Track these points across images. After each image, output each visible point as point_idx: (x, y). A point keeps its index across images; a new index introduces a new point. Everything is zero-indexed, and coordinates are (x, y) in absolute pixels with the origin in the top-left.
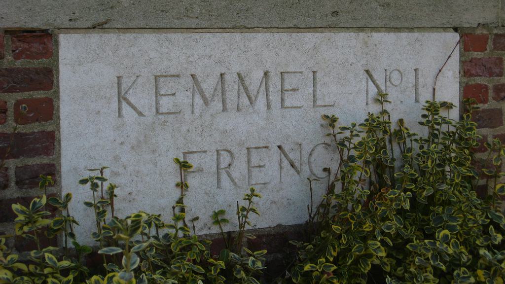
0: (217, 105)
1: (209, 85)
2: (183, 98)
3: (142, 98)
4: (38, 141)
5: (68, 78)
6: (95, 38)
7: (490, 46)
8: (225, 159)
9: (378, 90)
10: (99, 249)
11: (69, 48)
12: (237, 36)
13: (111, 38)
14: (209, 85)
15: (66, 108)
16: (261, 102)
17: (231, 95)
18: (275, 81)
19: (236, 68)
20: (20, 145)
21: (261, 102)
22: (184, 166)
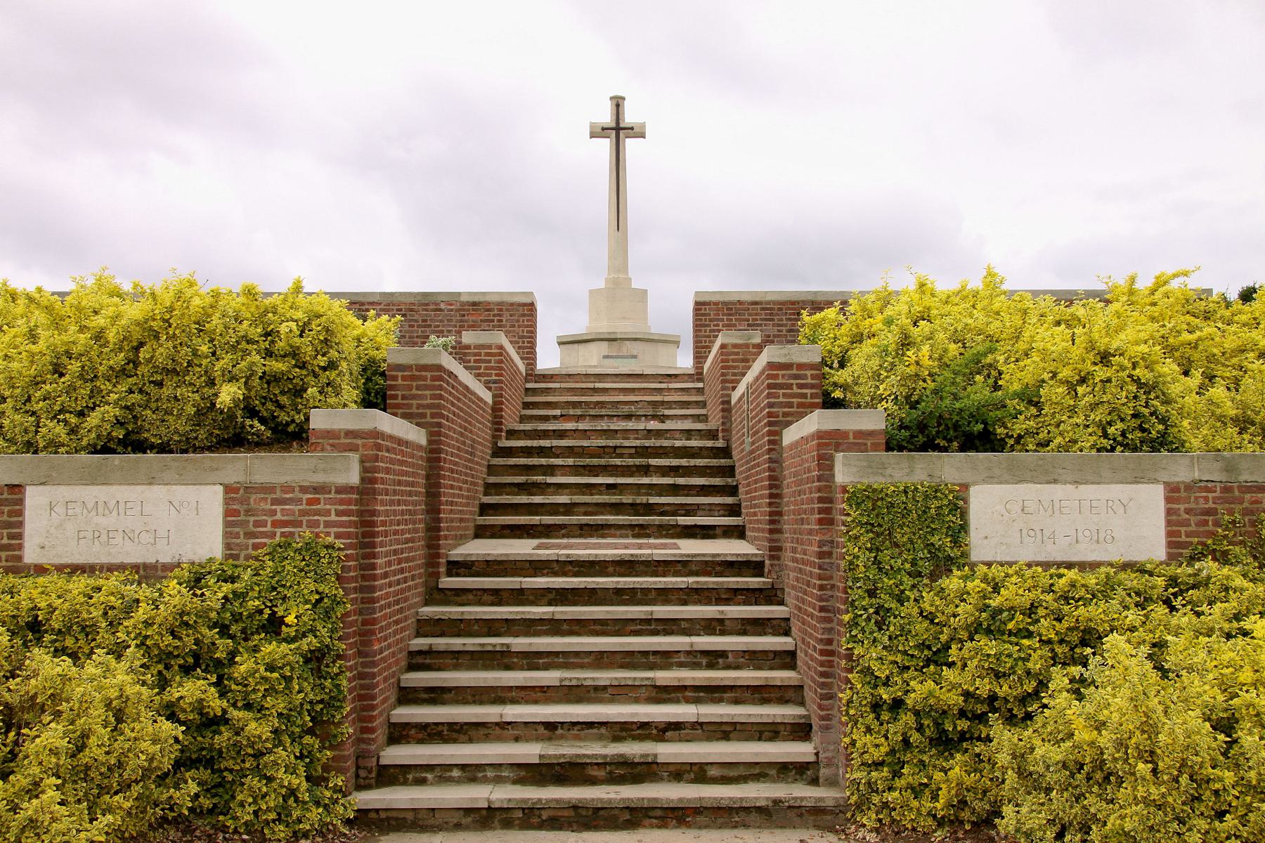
0: (94, 513)
1: (90, 506)
2: (78, 510)
3: (60, 509)
4: (15, 527)
5: (29, 502)
6: (41, 487)
7: (242, 491)
8: (97, 534)
9: (28, 567)
10: (985, 355)
11: (30, 492)
12: (104, 487)
13: (47, 488)
14: (90, 506)
15: (27, 513)
16: (115, 513)
17: (101, 509)
18: (122, 506)
19: (103, 499)
20: (10, 525)
21: (115, 513)
22: (618, 131)
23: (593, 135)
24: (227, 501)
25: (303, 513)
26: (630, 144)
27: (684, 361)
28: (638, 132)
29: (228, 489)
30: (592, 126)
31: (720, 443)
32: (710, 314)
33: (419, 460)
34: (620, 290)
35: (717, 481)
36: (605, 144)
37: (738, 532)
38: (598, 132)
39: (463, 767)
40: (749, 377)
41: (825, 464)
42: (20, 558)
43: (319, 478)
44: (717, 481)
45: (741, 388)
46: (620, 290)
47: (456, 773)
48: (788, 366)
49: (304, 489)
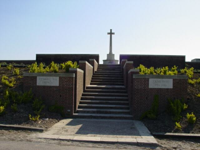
23: (108, 34)
24: (59, 79)
25: (68, 80)
26: (113, 35)
27: (119, 63)
28: (114, 34)
29: (60, 77)
30: (108, 33)
31: (122, 74)
32: (122, 57)
33: (83, 74)
34: (111, 55)
35: (121, 83)
36: (109, 35)
37: (123, 85)
38: (108, 33)
39: (87, 111)
40: (125, 65)
41: (132, 76)
42: (36, 85)
43: (70, 76)
44: (121, 83)
45: (124, 66)
46: (111, 55)
47: (86, 112)
48: (185, 80)
49: (68, 77)
